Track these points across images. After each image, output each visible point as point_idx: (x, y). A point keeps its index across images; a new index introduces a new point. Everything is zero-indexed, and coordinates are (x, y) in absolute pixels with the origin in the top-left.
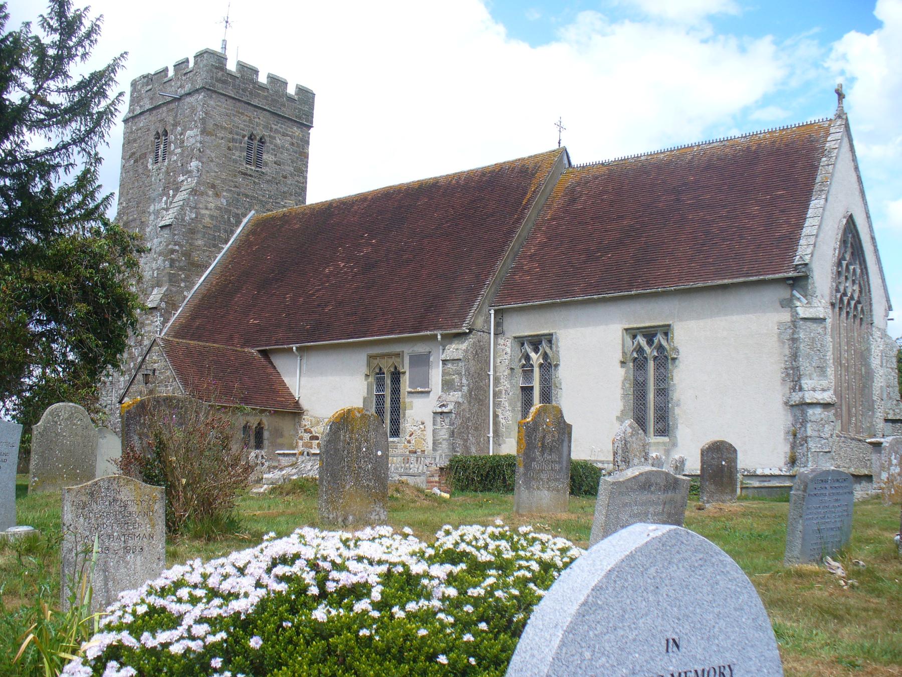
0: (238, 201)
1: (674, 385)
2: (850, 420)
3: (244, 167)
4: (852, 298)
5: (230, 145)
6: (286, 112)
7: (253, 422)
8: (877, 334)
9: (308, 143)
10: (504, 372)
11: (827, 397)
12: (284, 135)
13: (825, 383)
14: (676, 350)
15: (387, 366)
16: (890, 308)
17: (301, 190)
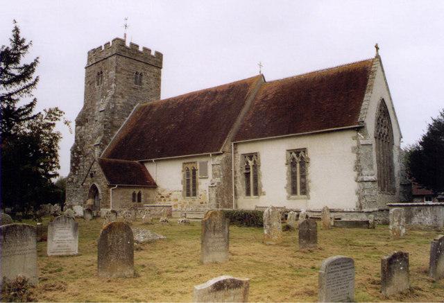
2: (385, 187)
6: (151, 62)
9: (160, 75)
10: (238, 169)
11: (373, 178)
12: (151, 72)
13: (372, 172)
14: (308, 159)
15: (190, 167)
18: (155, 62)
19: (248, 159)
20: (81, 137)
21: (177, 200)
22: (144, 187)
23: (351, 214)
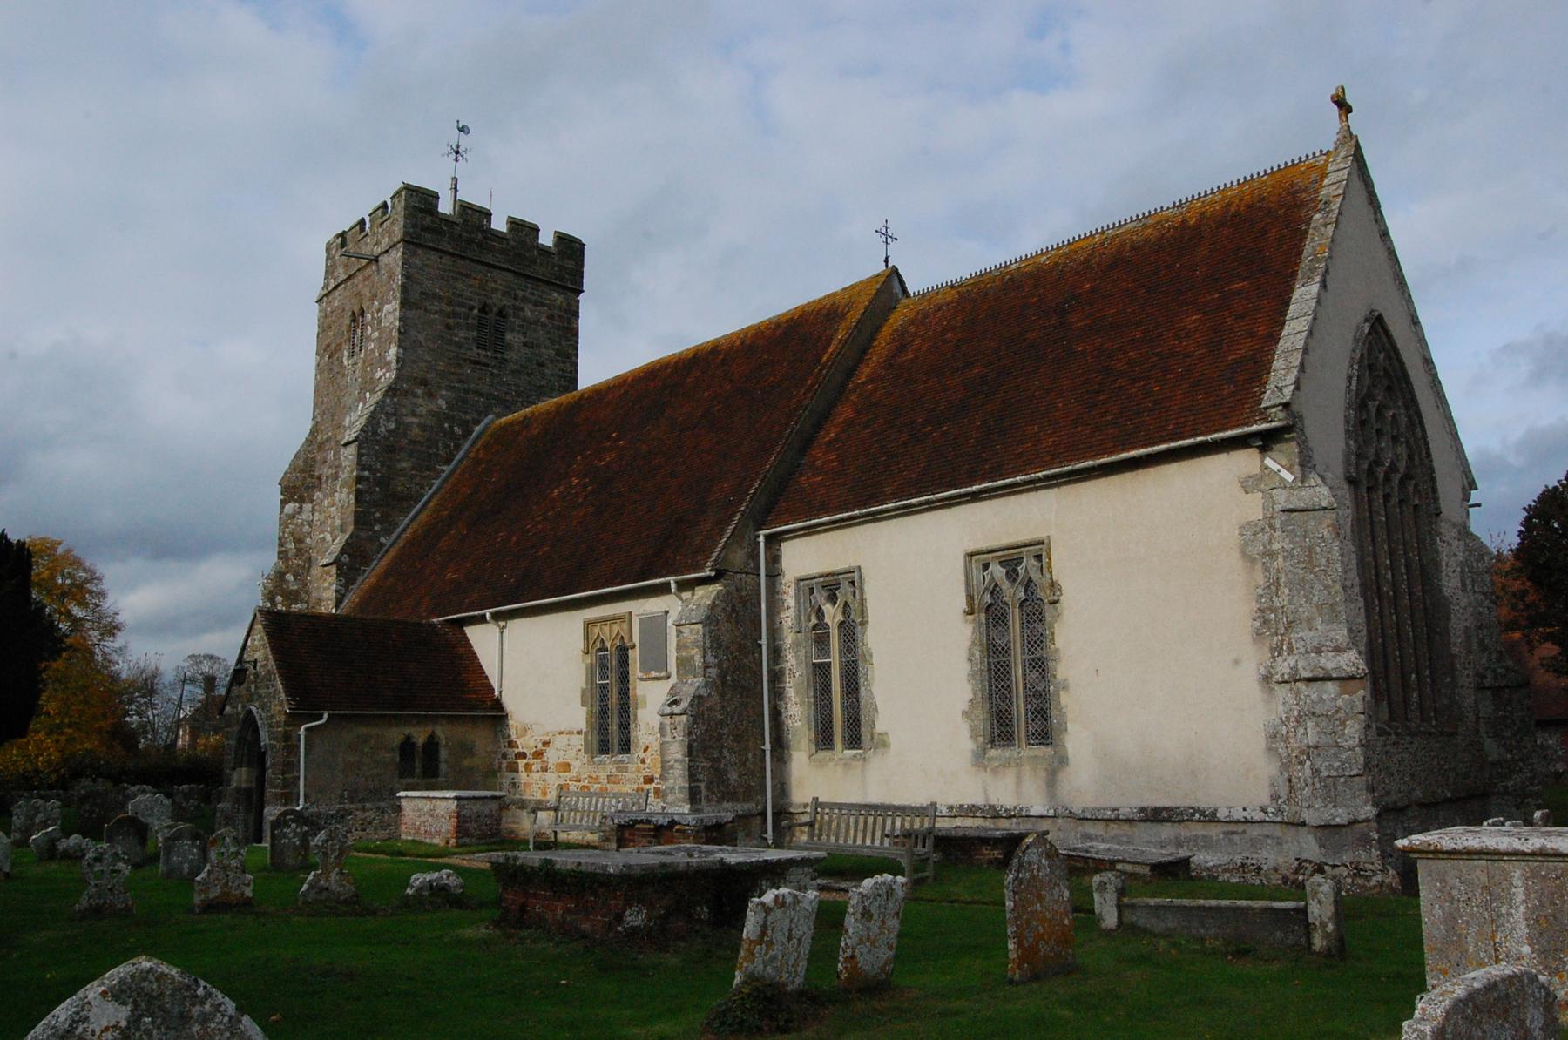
0: (465, 401)
1: (1057, 650)
2: (1406, 702)
3: (474, 352)
4: (1393, 468)
5: (451, 321)
6: (539, 270)
7: (420, 736)
8: (1448, 532)
9: (576, 315)
12: (536, 304)
16: (1472, 485)
17: (574, 380)
18: (564, 264)
19: (820, 597)
20: (299, 541)
21: (566, 767)
22: (450, 719)
23: (1255, 831)
